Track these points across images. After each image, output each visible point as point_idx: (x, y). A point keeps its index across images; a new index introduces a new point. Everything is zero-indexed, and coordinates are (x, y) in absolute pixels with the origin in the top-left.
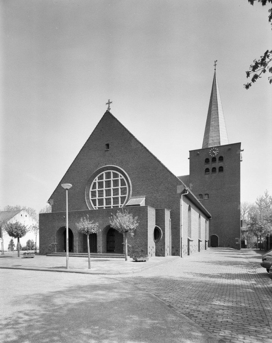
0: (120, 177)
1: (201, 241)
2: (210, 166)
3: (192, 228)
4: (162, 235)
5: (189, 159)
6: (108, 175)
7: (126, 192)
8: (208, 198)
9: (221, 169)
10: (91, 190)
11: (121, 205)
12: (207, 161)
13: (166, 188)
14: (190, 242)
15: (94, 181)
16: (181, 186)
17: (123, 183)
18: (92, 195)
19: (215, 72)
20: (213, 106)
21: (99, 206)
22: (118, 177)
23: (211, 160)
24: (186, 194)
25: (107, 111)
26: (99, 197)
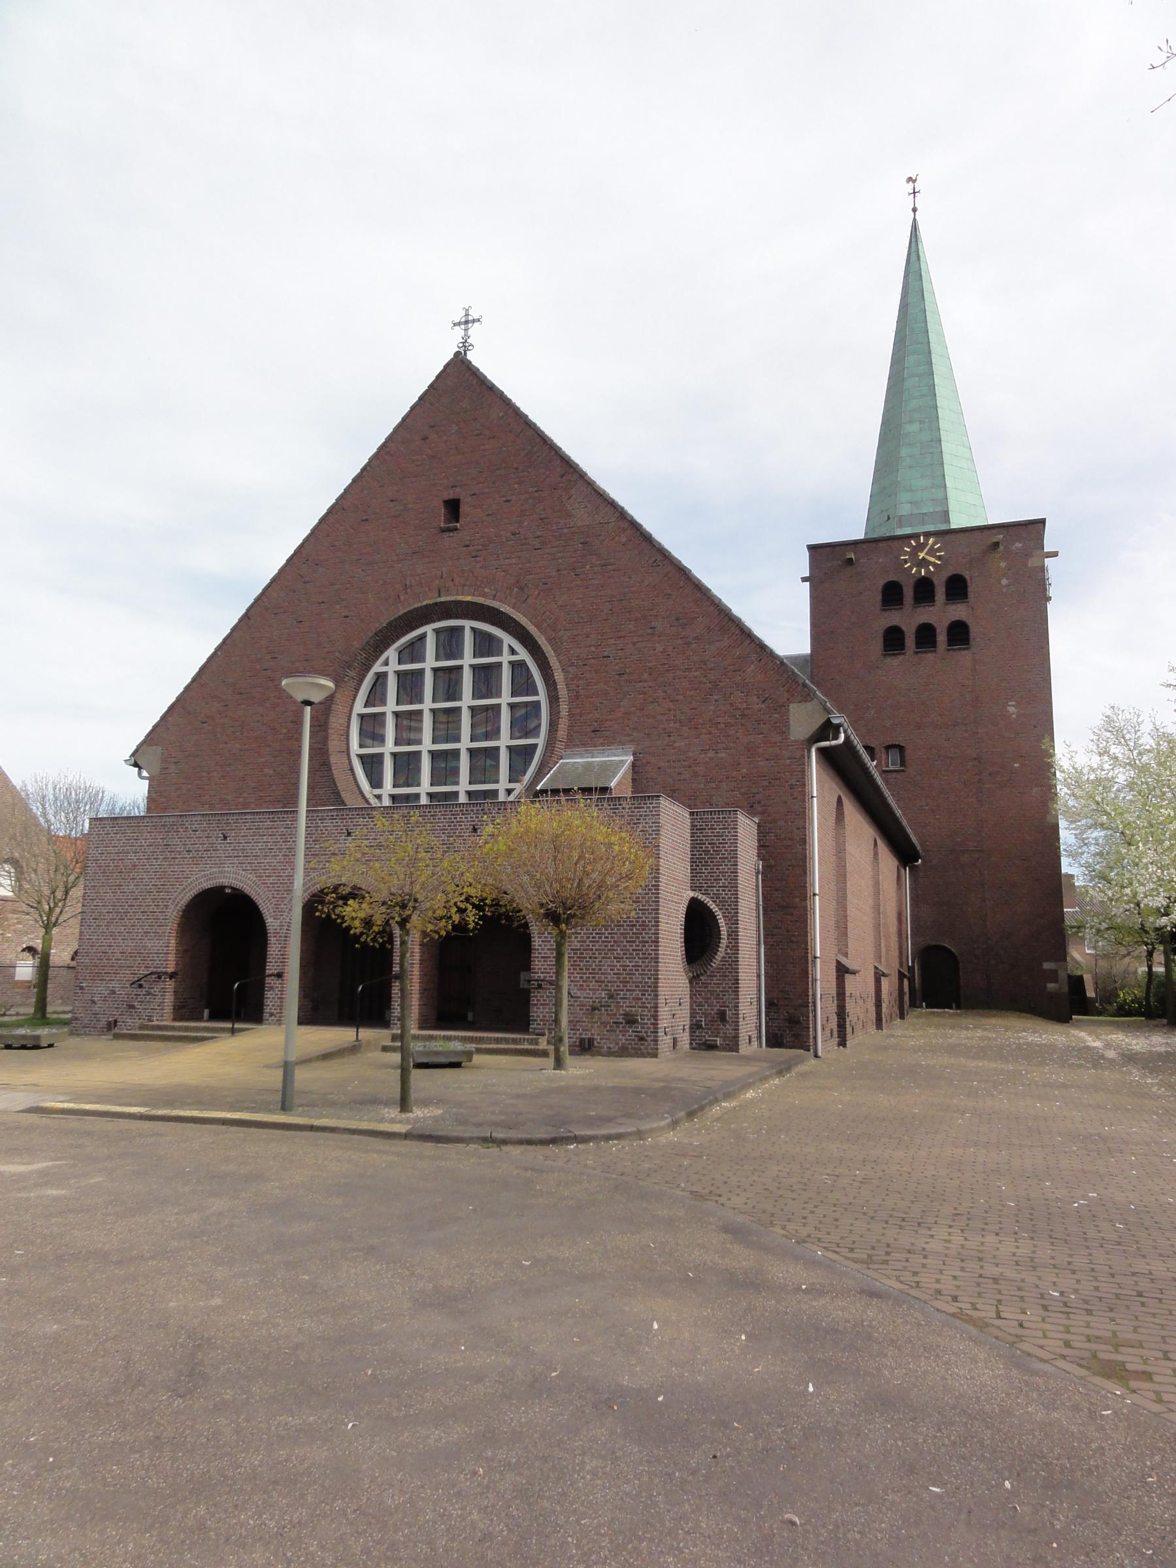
0: (511, 650)
1: (854, 973)
2: (909, 619)
3: (852, 912)
4: (724, 942)
5: (804, 580)
6: (450, 643)
7: (539, 725)
8: (903, 763)
9: (959, 634)
10: (359, 708)
11: (512, 786)
12: (892, 594)
13: (738, 713)
14: (848, 978)
15: (377, 668)
16: (810, 706)
17: (522, 684)
18: (362, 733)
19: (915, 219)
20: (910, 360)
21: (394, 786)
22: (500, 653)
23: (908, 593)
24: (834, 743)
25: (457, 354)
26: (396, 744)
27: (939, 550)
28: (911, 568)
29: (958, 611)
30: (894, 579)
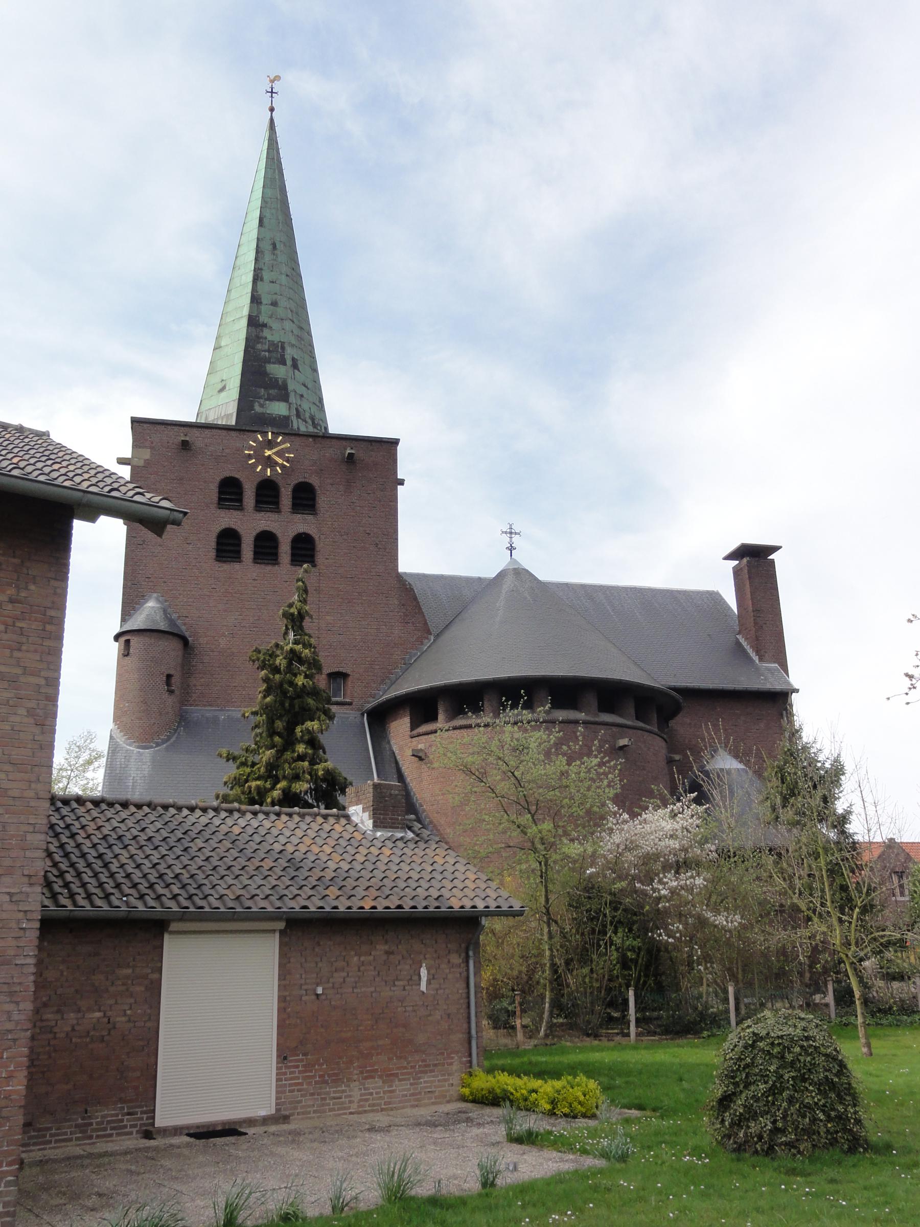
5: (402, 482)
27: (288, 450)
28: (254, 466)
29: (302, 524)
30: (236, 476)
